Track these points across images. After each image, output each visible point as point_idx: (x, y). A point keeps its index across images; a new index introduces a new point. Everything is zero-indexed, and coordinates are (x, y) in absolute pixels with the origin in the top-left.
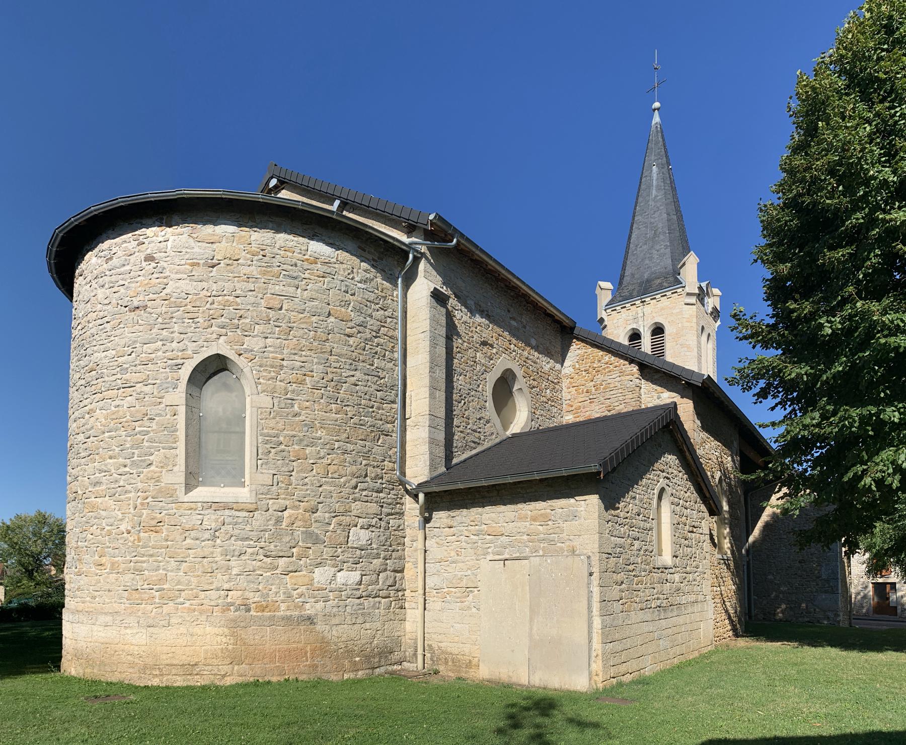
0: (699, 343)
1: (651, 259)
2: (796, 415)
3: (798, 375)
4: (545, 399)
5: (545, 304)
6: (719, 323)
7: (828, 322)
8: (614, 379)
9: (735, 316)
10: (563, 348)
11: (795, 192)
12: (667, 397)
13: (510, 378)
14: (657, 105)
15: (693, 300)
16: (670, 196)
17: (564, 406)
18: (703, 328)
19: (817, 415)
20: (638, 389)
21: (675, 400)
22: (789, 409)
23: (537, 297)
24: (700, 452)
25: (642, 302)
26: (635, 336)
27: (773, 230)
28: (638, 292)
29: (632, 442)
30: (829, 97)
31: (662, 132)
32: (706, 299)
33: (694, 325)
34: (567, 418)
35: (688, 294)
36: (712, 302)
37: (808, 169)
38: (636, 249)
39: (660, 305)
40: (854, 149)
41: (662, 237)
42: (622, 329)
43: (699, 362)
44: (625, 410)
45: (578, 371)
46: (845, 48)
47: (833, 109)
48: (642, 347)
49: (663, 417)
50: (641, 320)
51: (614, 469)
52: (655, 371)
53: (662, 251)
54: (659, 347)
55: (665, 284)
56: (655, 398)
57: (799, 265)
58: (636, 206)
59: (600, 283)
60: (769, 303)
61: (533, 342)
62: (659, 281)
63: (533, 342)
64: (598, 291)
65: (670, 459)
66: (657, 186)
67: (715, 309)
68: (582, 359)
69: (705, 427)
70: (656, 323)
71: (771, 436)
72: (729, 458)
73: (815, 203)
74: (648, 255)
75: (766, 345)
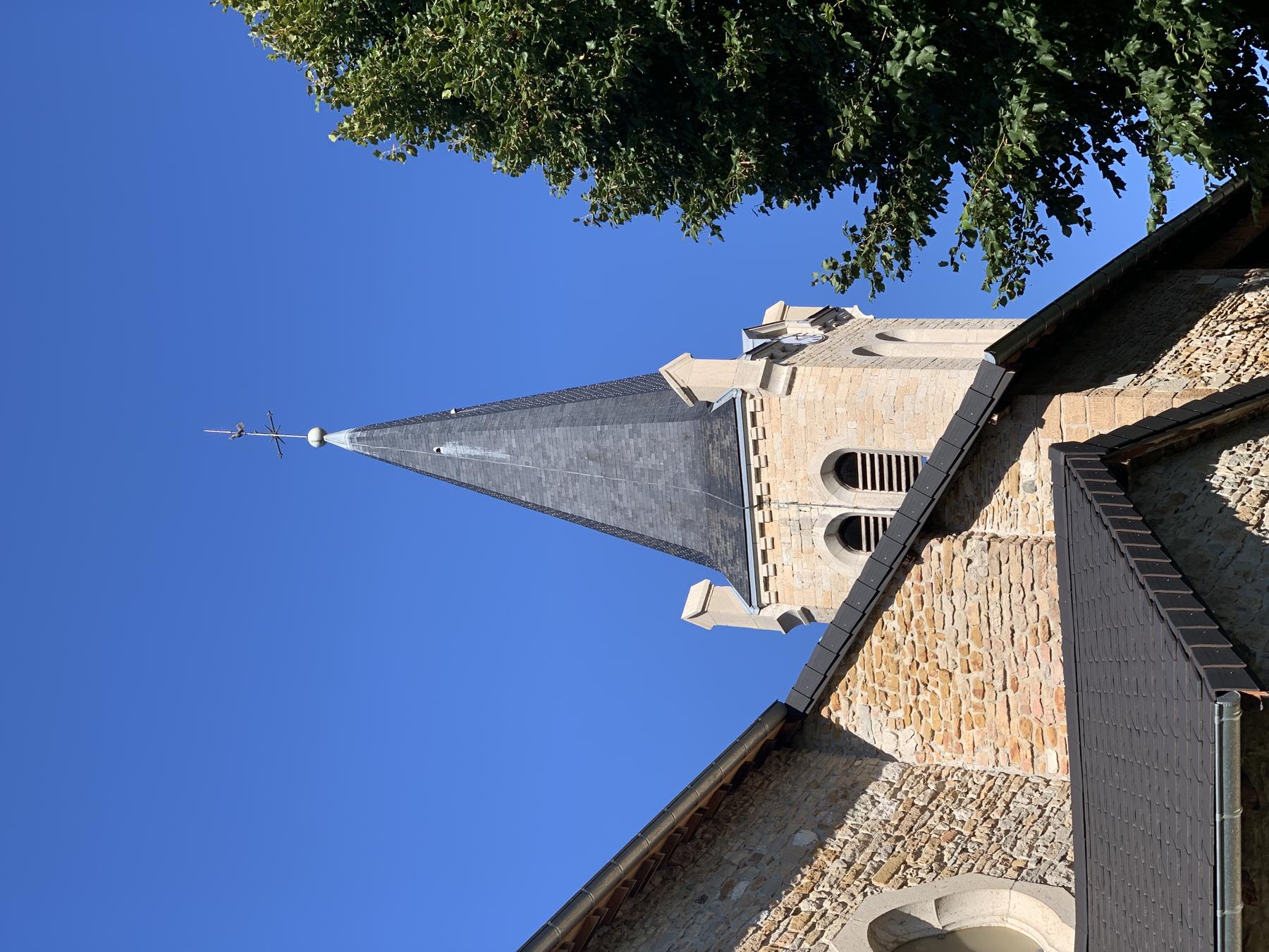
0: (897, 363)
1: (655, 473)
2: (1144, 125)
3: (1029, 124)
4: (982, 830)
5: (705, 786)
6: (854, 311)
7: (904, 52)
8: (957, 611)
9: (845, 281)
10: (840, 751)
11: (577, 142)
12: (1032, 466)
13: (898, 930)
15: (782, 373)
16: (517, 415)
17: (1012, 771)
18: (860, 351)
19: (1149, 77)
20: (996, 546)
21: (1046, 443)
22: (1126, 143)
23: (682, 808)
24: (1218, 382)
26: (848, 532)
27: (651, 190)
28: (731, 512)
29: (1155, 583)
30: (397, 76)
31: (373, 427)
32: (786, 340)
33: (848, 372)
34: (1052, 766)
35: (765, 384)
36: (797, 323)
37: (532, 116)
38: (623, 510)
39: (777, 459)
40: (515, 20)
41: (608, 443)
42: (821, 566)
43: (952, 364)
44: (1054, 587)
45: (915, 713)
46: (314, 45)
47: (423, 66)
48: (880, 514)
49: (1092, 486)
51: (1242, 651)
52: (954, 491)
53: (642, 443)
54: (891, 471)
55: (727, 442)
56: (1030, 498)
57: (742, 130)
58: (520, 503)
60: (824, 193)
61: (805, 837)
62: (715, 457)
63: (805, 837)
64: (705, 623)
65: (1231, 471)
66: (486, 446)
67: (815, 319)
68: (881, 699)
69: (1142, 363)
70: (824, 473)
71: (1192, 183)
72: (1250, 297)
73: (613, 96)
74: (645, 481)
75: (932, 201)
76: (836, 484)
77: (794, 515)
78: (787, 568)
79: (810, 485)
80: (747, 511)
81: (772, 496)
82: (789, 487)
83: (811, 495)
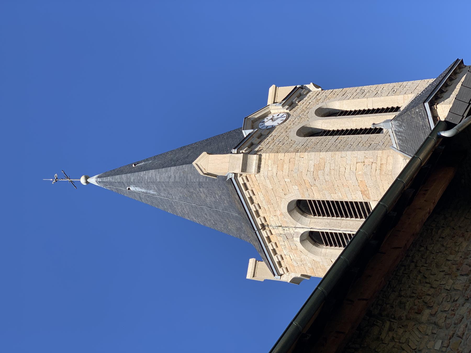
6: (310, 86)
14: (82, 180)
25: (263, 226)
35: (244, 169)
50: (287, 231)
59: (249, 276)
76: (299, 215)
77: (282, 232)
78: (287, 257)
79: (284, 217)
80: (257, 232)
81: (268, 222)
82: (275, 218)
83: (287, 222)
